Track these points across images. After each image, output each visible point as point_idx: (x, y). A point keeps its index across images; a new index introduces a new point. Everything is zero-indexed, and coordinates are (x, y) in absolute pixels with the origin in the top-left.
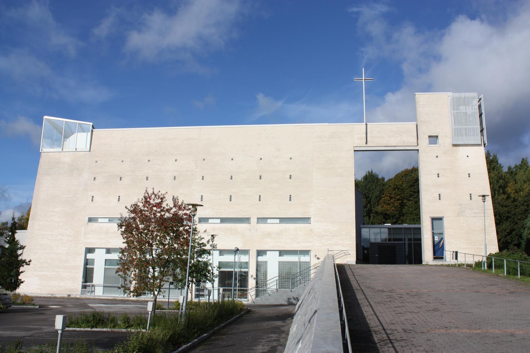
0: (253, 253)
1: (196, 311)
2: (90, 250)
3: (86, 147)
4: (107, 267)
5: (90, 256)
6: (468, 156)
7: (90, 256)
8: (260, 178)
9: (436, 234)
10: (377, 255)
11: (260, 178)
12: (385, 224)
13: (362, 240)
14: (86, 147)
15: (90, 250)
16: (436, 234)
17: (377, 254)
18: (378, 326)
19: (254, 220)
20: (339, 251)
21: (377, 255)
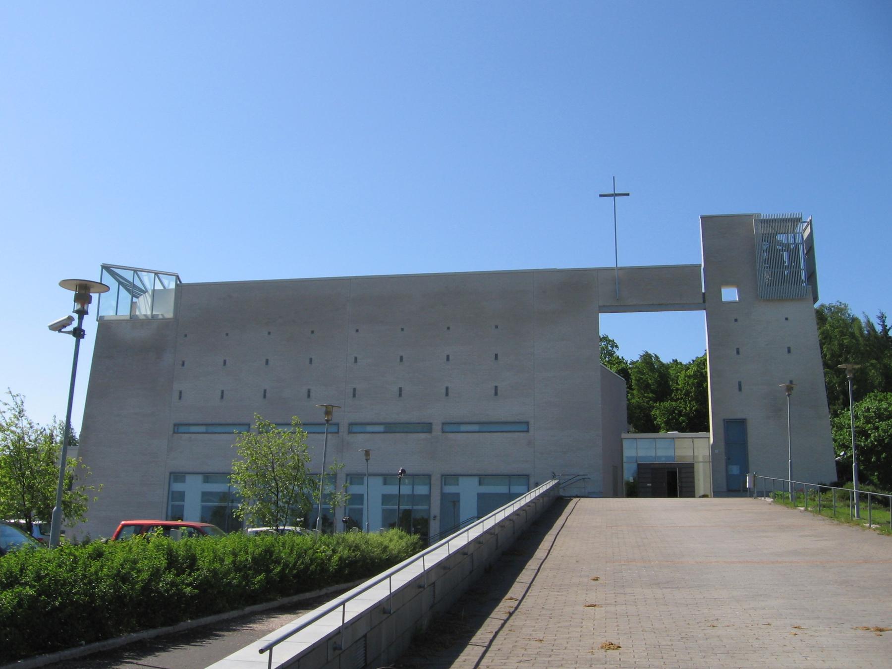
0: (436, 481)
1: (52, 584)
2: (178, 476)
3: (116, 314)
4: (181, 503)
5: (178, 487)
6: (787, 319)
7: (178, 487)
8: (496, 355)
9: (656, 454)
10: (649, 485)
11: (496, 355)
12: (668, 432)
13: (625, 460)
14: (116, 314)
15: (178, 476)
16: (656, 454)
17: (649, 483)
18: (625, 594)
19: (437, 428)
20: (573, 476)
21: (649, 485)
